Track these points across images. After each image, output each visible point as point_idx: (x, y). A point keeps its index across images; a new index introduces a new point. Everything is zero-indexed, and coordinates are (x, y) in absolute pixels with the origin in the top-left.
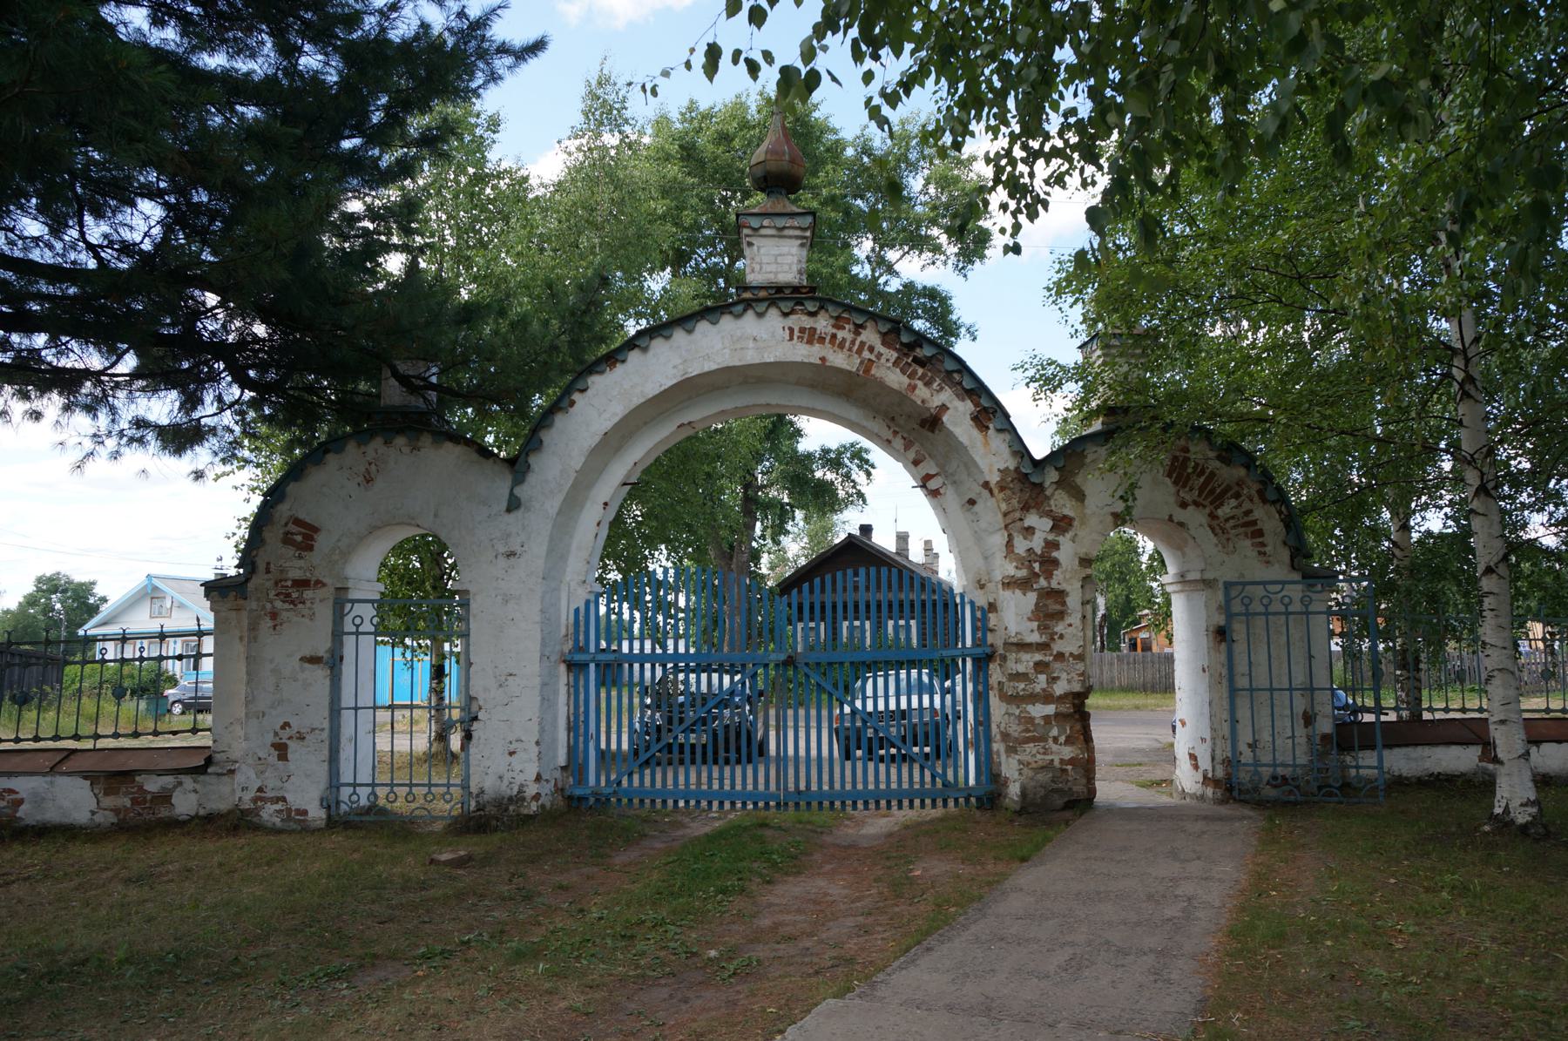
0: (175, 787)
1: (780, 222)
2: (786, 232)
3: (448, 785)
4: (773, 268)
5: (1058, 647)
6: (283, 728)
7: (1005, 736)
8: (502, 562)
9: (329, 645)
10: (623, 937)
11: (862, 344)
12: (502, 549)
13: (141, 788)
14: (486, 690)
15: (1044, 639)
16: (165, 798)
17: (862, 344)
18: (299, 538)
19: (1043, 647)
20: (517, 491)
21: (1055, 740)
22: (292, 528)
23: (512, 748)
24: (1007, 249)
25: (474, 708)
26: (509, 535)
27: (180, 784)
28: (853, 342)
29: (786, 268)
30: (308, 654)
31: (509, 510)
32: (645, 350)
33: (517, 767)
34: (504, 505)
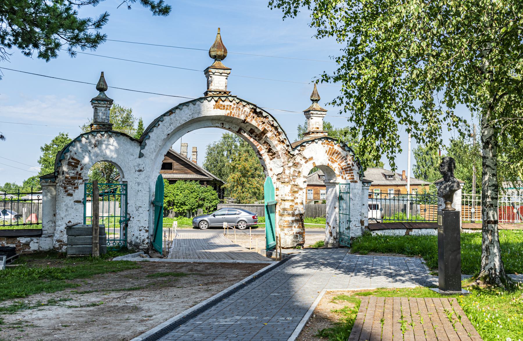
0: (30, 241)
1: (221, 71)
2: (223, 74)
3: (385, 199)
4: (218, 85)
5: (296, 201)
6: (69, 222)
7: (280, 226)
8: (137, 173)
9: (83, 197)
10: (93, 321)
11: (245, 111)
12: (137, 169)
13: (19, 241)
14: (132, 211)
15: (293, 199)
16: (27, 245)
17: (245, 111)
18: (73, 164)
19: (293, 201)
20: (142, 151)
21: (295, 227)
22: (71, 160)
23: (141, 228)
24: (306, 162)
25: (128, 217)
26: (139, 165)
27: (32, 240)
28: (242, 110)
29: (222, 85)
30: (76, 200)
31: (140, 157)
32: (181, 109)
33: (142, 234)
34: (138, 155)
